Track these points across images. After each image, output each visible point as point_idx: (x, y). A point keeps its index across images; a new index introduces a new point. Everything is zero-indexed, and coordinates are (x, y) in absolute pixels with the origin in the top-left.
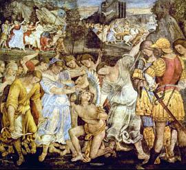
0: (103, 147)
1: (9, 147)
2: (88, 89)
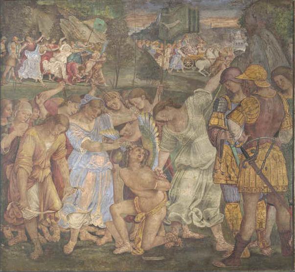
0: (162, 233)
2: (139, 142)
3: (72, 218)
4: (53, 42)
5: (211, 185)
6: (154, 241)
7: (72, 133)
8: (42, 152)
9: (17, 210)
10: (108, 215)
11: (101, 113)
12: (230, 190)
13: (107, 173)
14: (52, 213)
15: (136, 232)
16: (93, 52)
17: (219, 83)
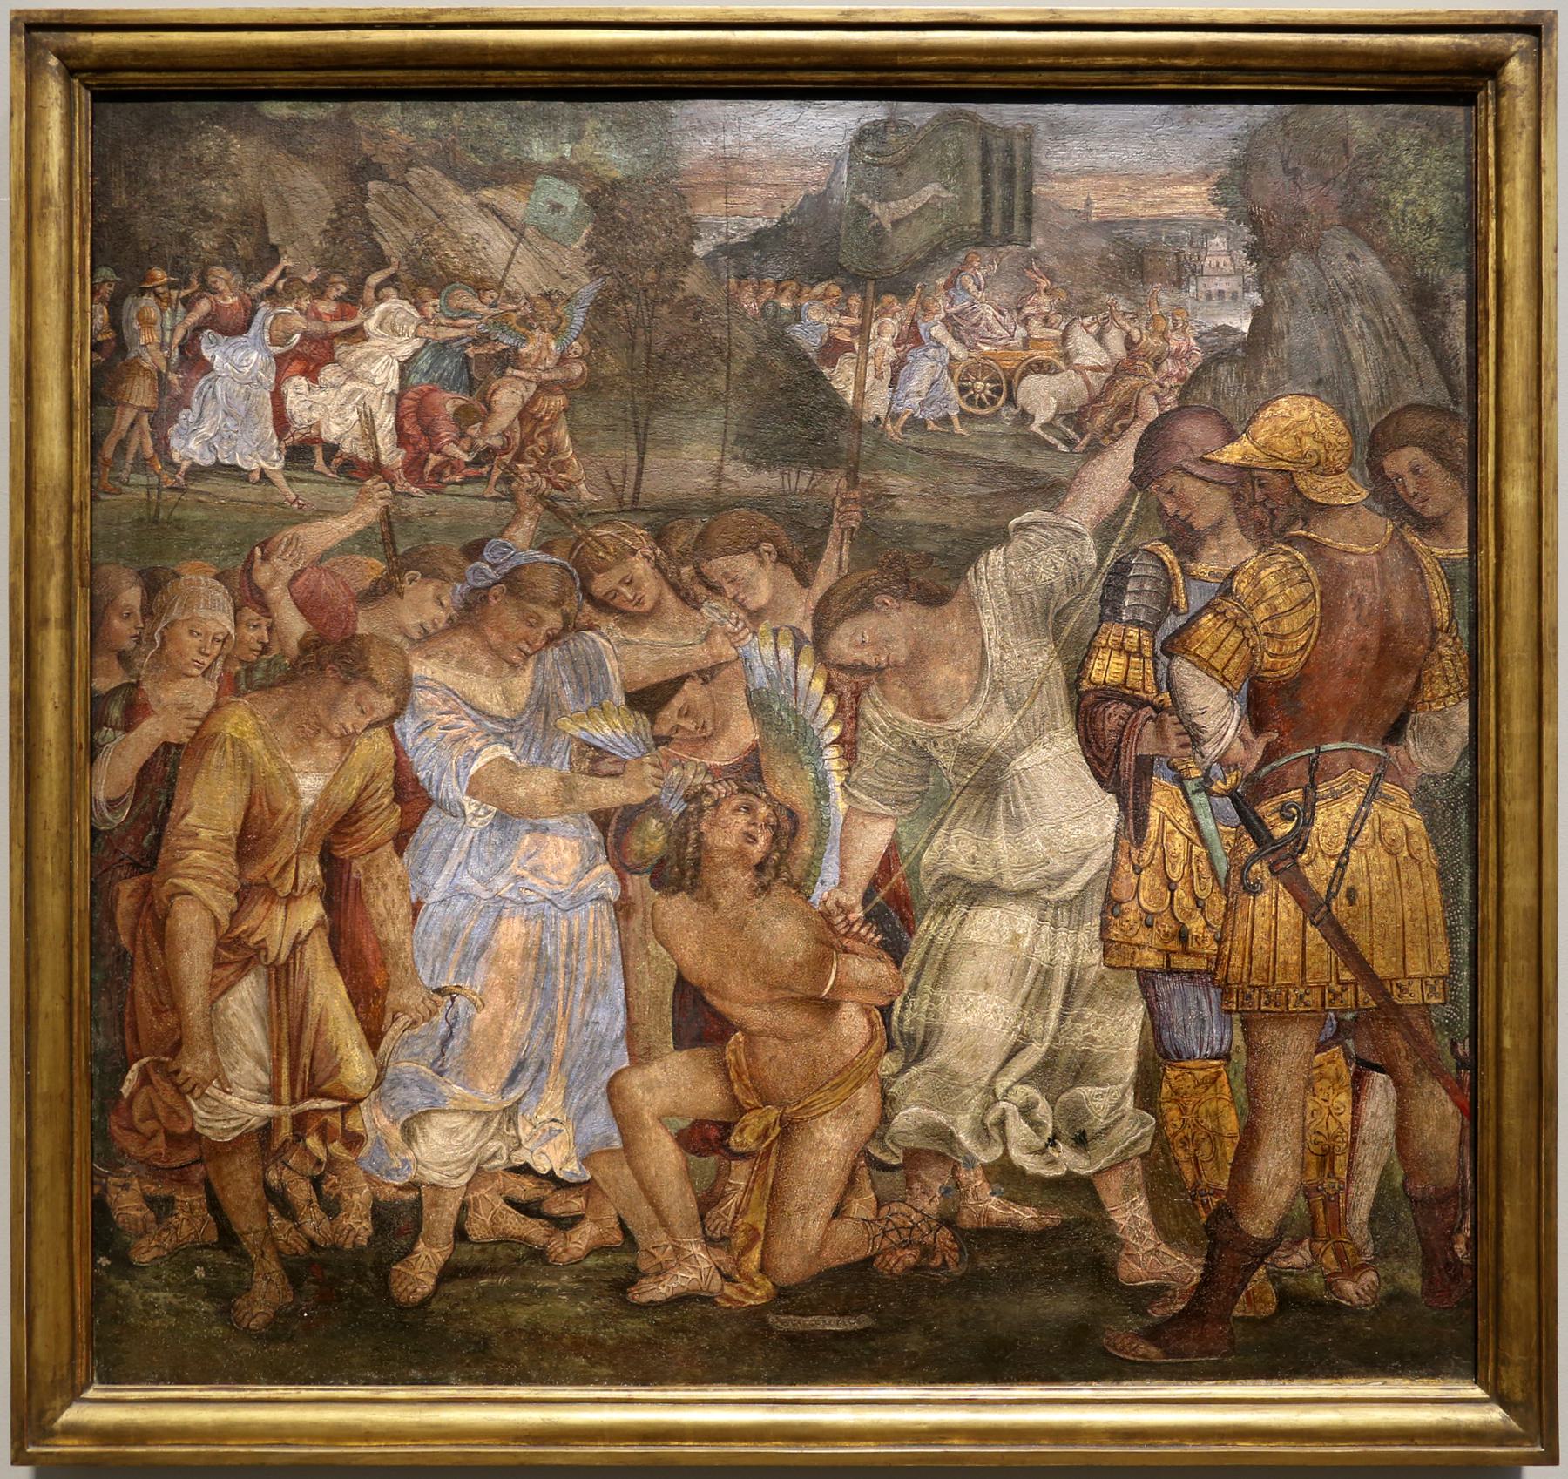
0: (862, 1206)
1: (183, 1197)
2: (750, 771)
3: (425, 1135)
4: (333, 293)
5: (1091, 975)
6: (823, 1245)
7: (425, 727)
8: (281, 818)
9: (169, 1096)
10: (600, 1123)
11: (565, 629)
12: (1185, 1002)
13: (594, 923)
14: (335, 1110)
15: (732, 1202)
16: (525, 339)
17: (1128, 484)
